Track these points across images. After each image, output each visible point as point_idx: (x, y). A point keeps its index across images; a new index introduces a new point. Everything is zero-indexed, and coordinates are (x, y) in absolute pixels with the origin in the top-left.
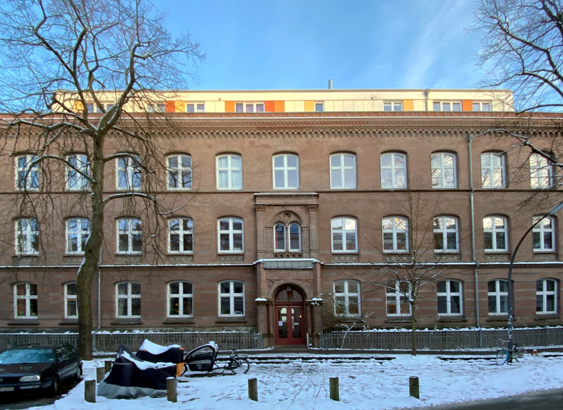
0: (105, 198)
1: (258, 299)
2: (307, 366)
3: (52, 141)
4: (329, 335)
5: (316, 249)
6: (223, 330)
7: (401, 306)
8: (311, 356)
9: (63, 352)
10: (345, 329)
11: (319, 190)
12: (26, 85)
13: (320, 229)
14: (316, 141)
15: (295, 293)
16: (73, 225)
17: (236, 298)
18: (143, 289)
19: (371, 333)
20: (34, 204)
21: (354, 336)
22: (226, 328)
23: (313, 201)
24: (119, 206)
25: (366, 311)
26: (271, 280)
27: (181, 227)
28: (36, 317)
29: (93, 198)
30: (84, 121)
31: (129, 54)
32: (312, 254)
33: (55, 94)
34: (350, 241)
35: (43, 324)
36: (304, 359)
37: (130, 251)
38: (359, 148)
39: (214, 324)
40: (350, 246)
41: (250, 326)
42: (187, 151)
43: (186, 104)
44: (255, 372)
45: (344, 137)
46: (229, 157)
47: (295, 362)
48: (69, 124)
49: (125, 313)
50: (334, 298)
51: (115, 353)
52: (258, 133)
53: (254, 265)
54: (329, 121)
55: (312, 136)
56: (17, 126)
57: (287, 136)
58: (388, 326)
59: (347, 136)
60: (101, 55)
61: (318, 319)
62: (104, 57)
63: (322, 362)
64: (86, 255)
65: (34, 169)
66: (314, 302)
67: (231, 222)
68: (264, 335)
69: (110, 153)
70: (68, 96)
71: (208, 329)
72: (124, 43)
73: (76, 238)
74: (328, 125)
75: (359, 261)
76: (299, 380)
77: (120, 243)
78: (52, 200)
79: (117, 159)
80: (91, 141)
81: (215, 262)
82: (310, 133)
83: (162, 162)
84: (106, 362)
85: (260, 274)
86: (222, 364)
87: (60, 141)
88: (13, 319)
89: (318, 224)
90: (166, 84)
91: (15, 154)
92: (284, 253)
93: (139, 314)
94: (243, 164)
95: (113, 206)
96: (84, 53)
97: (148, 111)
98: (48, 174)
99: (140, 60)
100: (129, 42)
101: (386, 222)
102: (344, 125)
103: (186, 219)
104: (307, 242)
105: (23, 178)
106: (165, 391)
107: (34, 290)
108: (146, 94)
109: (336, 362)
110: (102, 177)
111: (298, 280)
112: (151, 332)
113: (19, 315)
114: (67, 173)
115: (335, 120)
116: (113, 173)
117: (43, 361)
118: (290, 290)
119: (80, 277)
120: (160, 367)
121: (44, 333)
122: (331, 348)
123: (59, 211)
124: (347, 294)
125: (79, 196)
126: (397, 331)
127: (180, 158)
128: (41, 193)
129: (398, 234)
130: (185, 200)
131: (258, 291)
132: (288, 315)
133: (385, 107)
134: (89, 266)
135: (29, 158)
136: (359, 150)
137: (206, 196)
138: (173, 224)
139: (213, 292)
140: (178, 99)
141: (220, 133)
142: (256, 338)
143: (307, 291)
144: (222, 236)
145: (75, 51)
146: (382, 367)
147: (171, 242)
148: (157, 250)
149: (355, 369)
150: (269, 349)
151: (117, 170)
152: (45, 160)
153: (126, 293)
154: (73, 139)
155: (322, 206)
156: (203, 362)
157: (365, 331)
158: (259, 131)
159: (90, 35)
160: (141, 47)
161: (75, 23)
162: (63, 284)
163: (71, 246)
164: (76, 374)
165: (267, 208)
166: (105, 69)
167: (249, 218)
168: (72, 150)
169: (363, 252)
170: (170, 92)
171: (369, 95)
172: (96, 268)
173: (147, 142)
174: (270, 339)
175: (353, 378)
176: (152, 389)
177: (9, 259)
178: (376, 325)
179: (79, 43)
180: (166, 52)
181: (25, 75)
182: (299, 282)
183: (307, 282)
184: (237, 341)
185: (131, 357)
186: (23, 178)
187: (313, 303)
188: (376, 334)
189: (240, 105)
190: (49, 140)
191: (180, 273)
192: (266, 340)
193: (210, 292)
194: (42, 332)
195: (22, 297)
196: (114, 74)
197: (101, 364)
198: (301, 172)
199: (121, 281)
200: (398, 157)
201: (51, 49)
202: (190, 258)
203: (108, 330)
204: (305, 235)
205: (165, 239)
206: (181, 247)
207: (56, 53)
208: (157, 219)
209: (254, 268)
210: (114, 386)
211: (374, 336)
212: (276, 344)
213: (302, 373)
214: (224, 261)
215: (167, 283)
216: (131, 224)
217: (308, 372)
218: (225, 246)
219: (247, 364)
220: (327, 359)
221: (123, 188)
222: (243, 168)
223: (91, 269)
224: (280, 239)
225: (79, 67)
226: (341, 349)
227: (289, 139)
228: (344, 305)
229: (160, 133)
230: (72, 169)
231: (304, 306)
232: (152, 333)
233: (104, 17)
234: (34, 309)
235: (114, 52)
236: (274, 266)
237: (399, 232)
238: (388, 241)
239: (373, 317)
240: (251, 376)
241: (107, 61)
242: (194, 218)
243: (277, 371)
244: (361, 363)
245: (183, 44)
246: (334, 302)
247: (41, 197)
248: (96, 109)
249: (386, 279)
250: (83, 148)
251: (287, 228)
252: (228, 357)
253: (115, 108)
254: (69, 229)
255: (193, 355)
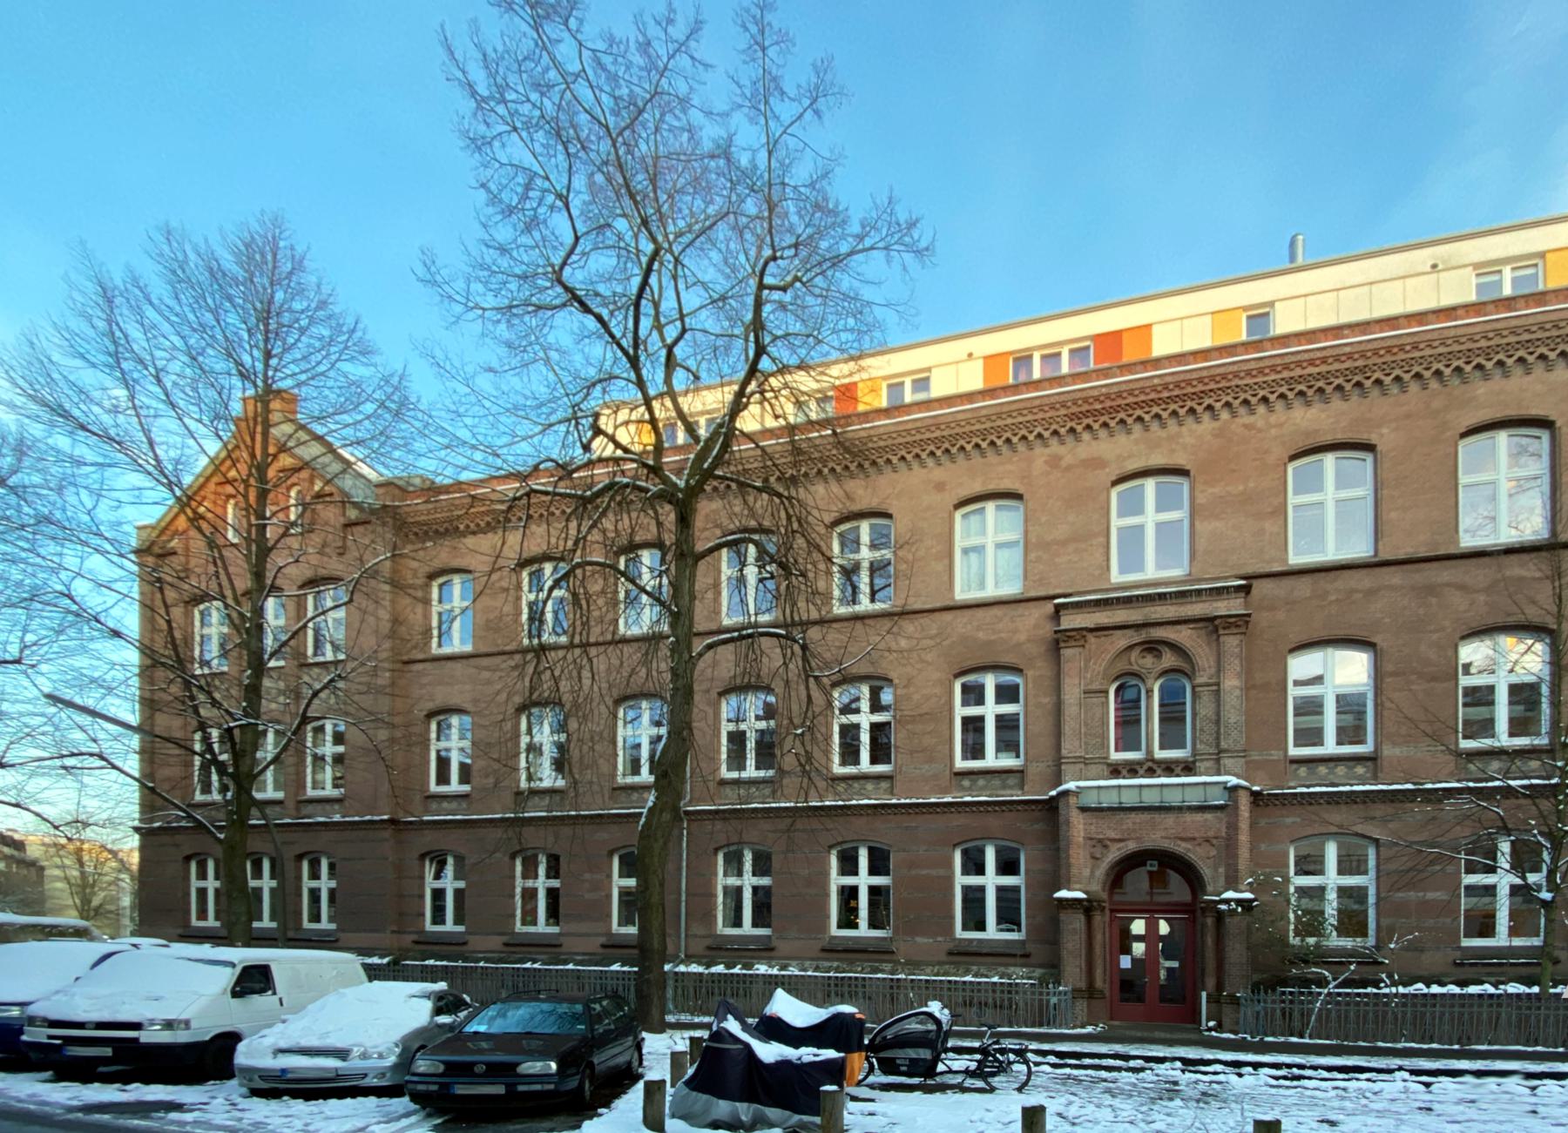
0: (698, 645)
1: (1063, 894)
2: (1196, 1082)
3: (592, 527)
4: (1270, 997)
5: (1239, 747)
6: (966, 973)
7: (1512, 916)
8: (1210, 1057)
9: (606, 1012)
10: (1322, 982)
11: (1250, 570)
12: (542, 405)
13: (1254, 687)
14: (1245, 426)
15: (1175, 878)
16: (631, 714)
17: (1001, 890)
18: (776, 863)
19: (1404, 995)
20: (557, 673)
21: (1348, 1004)
22: (975, 968)
23: (1222, 607)
24: (725, 663)
25: (1391, 931)
26: (1100, 841)
27: (865, 705)
28: (555, 930)
29: (672, 650)
30: (656, 470)
31: (753, 283)
32: (1227, 762)
33: (597, 416)
34: (1349, 718)
35: (569, 944)
36: (1186, 1062)
37: (751, 771)
38: (1385, 431)
39: (944, 958)
40: (1349, 734)
41: (1040, 966)
42: (883, 508)
43: (884, 385)
44: (1047, 1089)
45: (1337, 403)
46: (990, 506)
47: (1162, 1069)
48: (625, 480)
49: (738, 923)
50: (1292, 890)
51: (706, 1019)
52: (1072, 430)
53: (1052, 798)
54: (1287, 360)
55: (1234, 415)
56: (524, 501)
57: (1155, 426)
58: (1463, 977)
59: (1345, 398)
60: (692, 299)
61: (1236, 953)
62: (697, 305)
63: (1240, 1075)
64: (656, 785)
65: (557, 593)
66: (1227, 901)
67: (990, 682)
68: (1076, 992)
69: (708, 540)
70: (623, 415)
71: (929, 970)
72: (742, 258)
73: (639, 745)
74: (1286, 374)
75: (1375, 779)
76: (1170, 1120)
77: (729, 751)
78: (590, 660)
79: (724, 551)
80: (669, 515)
81: (946, 792)
82: (1228, 404)
83: (822, 544)
84: (691, 1039)
85: (1068, 822)
86: (960, 1063)
87: (608, 523)
88: (513, 933)
89: (1247, 672)
90: (836, 344)
91: (523, 564)
92: (1140, 763)
93: (768, 926)
94: (1026, 521)
95: (715, 664)
96: (656, 305)
97: (792, 420)
98: (584, 602)
99: (776, 295)
100: (753, 253)
101: (1473, 652)
102: (1337, 366)
103: (877, 683)
104: (1210, 728)
105: (536, 617)
106: (817, 1120)
107: (553, 872)
108: (788, 378)
109: (1285, 1078)
110: (693, 598)
111: (1182, 839)
112: (794, 971)
113: (524, 923)
114: (622, 596)
115: (1306, 356)
116: (716, 586)
117: (565, 1030)
118: (1157, 871)
119: (646, 834)
120: (806, 1059)
121: (571, 966)
122: (1273, 1035)
123: (604, 685)
124: (1332, 878)
125: (644, 646)
126: (1491, 989)
127: (865, 527)
128: (571, 646)
129: (1515, 689)
130: (873, 636)
131: (1063, 871)
132: (1150, 936)
133: (1479, 286)
134: (662, 811)
135: (548, 568)
136: (1384, 437)
137: (925, 620)
138: (846, 700)
139: (941, 872)
140: (865, 376)
141: (969, 447)
142: (1054, 1000)
143: (1206, 872)
144: (966, 721)
145: (637, 305)
146: (1428, 1097)
147: (841, 745)
148: (809, 768)
149: (1343, 1098)
150: (1089, 1029)
151: (724, 578)
152: (579, 572)
153: (740, 874)
154: (634, 515)
155: (1261, 619)
156: (912, 1053)
157: (1386, 991)
158: (1073, 424)
159: (669, 257)
160: (780, 262)
161: (636, 236)
162: (611, 854)
163: (629, 766)
164: (629, 1063)
165: (1090, 637)
166: (699, 335)
167: (1039, 669)
168: (631, 541)
169: (1387, 751)
170: (846, 361)
171: (1423, 257)
172: (677, 815)
173: (789, 498)
174: (1094, 1002)
175: (1333, 1123)
176: (787, 1113)
177: (508, 798)
178: (1425, 973)
179: (645, 283)
180: (837, 261)
181: (538, 382)
182: (1184, 844)
183: (1206, 846)
184: (1003, 1005)
185: (744, 1030)
186: (536, 617)
187: (1223, 907)
188: (1420, 1001)
189: (1023, 359)
190: (586, 524)
191: (859, 823)
192: (1081, 1006)
193: (934, 872)
194: (566, 962)
195: (530, 883)
196: (720, 342)
197: (680, 1042)
198: (1197, 523)
199: (728, 845)
200: (1525, 441)
201: (586, 309)
202: (884, 785)
203: (699, 964)
204: (1206, 708)
205: (828, 738)
206: (865, 755)
207: (599, 318)
208: (807, 688)
209: (1051, 809)
210: (705, 1097)
211: (1414, 1005)
212: (1112, 1019)
213: (1178, 1102)
214: (970, 789)
215: (831, 847)
216: (753, 704)
217: (1198, 1101)
218: (975, 749)
219: (1024, 1068)
220: (1256, 1066)
221: (738, 619)
222: (1026, 532)
223: (666, 816)
224: (1129, 722)
225: (645, 342)
226: (1307, 1041)
227: (1163, 434)
228: (1322, 912)
229: (820, 472)
230: (630, 586)
231: (1195, 914)
232: (797, 973)
233: (699, 203)
234: (553, 914)
235: (718, 288)
236: (1109, 800)
237: (1514, 679)
238: (1479, 712)
239: (1416, 949)
240: (1032, 1099)
241: (704, 314)
242: (896, 681)
243: (1108, 1091)
244: (1364, 1084)
245: (877, 230)
246: (1288, 902)
247: (569, 656)
248: (681, 437)
249: (1463, 833)
250: (651, 533)
251: (1149, 692)
252: (977, 1044)
253: (721, 426)
254: (625, 723)
255: (889, 1034)
